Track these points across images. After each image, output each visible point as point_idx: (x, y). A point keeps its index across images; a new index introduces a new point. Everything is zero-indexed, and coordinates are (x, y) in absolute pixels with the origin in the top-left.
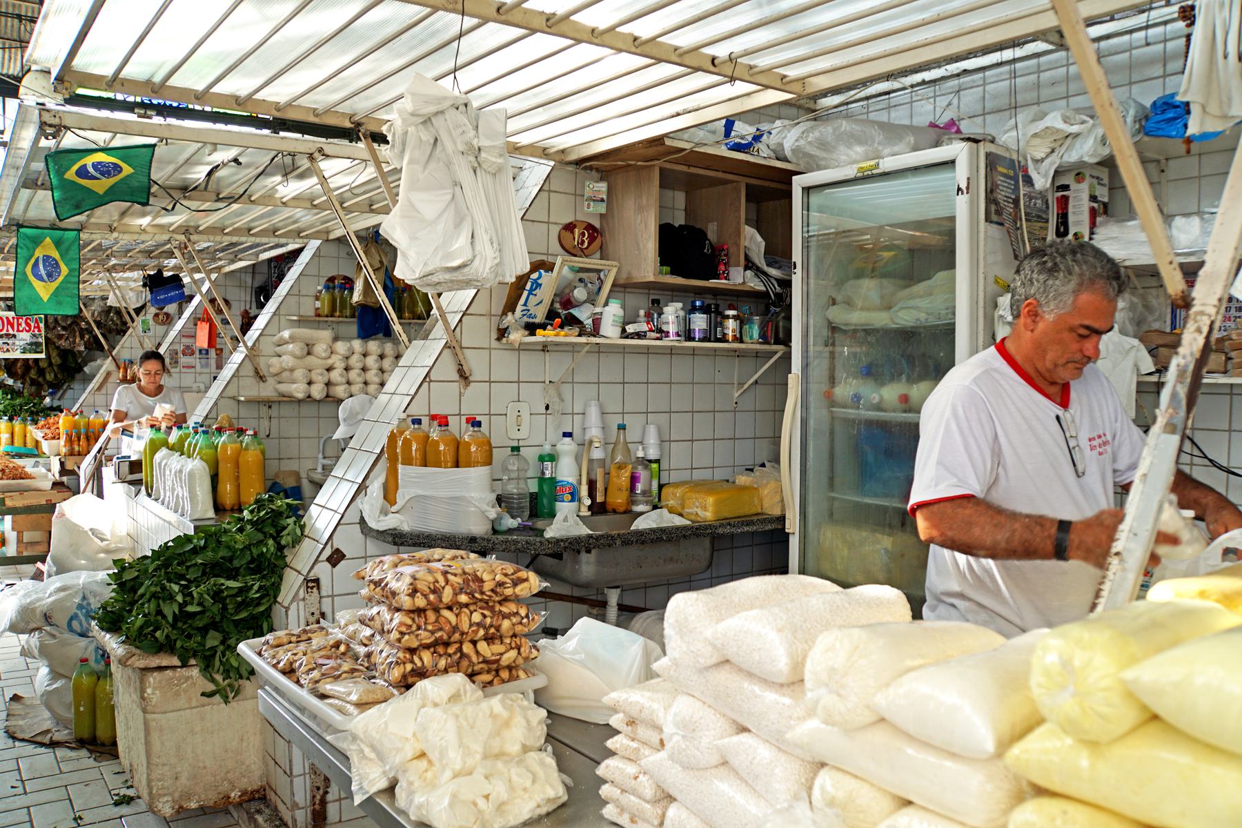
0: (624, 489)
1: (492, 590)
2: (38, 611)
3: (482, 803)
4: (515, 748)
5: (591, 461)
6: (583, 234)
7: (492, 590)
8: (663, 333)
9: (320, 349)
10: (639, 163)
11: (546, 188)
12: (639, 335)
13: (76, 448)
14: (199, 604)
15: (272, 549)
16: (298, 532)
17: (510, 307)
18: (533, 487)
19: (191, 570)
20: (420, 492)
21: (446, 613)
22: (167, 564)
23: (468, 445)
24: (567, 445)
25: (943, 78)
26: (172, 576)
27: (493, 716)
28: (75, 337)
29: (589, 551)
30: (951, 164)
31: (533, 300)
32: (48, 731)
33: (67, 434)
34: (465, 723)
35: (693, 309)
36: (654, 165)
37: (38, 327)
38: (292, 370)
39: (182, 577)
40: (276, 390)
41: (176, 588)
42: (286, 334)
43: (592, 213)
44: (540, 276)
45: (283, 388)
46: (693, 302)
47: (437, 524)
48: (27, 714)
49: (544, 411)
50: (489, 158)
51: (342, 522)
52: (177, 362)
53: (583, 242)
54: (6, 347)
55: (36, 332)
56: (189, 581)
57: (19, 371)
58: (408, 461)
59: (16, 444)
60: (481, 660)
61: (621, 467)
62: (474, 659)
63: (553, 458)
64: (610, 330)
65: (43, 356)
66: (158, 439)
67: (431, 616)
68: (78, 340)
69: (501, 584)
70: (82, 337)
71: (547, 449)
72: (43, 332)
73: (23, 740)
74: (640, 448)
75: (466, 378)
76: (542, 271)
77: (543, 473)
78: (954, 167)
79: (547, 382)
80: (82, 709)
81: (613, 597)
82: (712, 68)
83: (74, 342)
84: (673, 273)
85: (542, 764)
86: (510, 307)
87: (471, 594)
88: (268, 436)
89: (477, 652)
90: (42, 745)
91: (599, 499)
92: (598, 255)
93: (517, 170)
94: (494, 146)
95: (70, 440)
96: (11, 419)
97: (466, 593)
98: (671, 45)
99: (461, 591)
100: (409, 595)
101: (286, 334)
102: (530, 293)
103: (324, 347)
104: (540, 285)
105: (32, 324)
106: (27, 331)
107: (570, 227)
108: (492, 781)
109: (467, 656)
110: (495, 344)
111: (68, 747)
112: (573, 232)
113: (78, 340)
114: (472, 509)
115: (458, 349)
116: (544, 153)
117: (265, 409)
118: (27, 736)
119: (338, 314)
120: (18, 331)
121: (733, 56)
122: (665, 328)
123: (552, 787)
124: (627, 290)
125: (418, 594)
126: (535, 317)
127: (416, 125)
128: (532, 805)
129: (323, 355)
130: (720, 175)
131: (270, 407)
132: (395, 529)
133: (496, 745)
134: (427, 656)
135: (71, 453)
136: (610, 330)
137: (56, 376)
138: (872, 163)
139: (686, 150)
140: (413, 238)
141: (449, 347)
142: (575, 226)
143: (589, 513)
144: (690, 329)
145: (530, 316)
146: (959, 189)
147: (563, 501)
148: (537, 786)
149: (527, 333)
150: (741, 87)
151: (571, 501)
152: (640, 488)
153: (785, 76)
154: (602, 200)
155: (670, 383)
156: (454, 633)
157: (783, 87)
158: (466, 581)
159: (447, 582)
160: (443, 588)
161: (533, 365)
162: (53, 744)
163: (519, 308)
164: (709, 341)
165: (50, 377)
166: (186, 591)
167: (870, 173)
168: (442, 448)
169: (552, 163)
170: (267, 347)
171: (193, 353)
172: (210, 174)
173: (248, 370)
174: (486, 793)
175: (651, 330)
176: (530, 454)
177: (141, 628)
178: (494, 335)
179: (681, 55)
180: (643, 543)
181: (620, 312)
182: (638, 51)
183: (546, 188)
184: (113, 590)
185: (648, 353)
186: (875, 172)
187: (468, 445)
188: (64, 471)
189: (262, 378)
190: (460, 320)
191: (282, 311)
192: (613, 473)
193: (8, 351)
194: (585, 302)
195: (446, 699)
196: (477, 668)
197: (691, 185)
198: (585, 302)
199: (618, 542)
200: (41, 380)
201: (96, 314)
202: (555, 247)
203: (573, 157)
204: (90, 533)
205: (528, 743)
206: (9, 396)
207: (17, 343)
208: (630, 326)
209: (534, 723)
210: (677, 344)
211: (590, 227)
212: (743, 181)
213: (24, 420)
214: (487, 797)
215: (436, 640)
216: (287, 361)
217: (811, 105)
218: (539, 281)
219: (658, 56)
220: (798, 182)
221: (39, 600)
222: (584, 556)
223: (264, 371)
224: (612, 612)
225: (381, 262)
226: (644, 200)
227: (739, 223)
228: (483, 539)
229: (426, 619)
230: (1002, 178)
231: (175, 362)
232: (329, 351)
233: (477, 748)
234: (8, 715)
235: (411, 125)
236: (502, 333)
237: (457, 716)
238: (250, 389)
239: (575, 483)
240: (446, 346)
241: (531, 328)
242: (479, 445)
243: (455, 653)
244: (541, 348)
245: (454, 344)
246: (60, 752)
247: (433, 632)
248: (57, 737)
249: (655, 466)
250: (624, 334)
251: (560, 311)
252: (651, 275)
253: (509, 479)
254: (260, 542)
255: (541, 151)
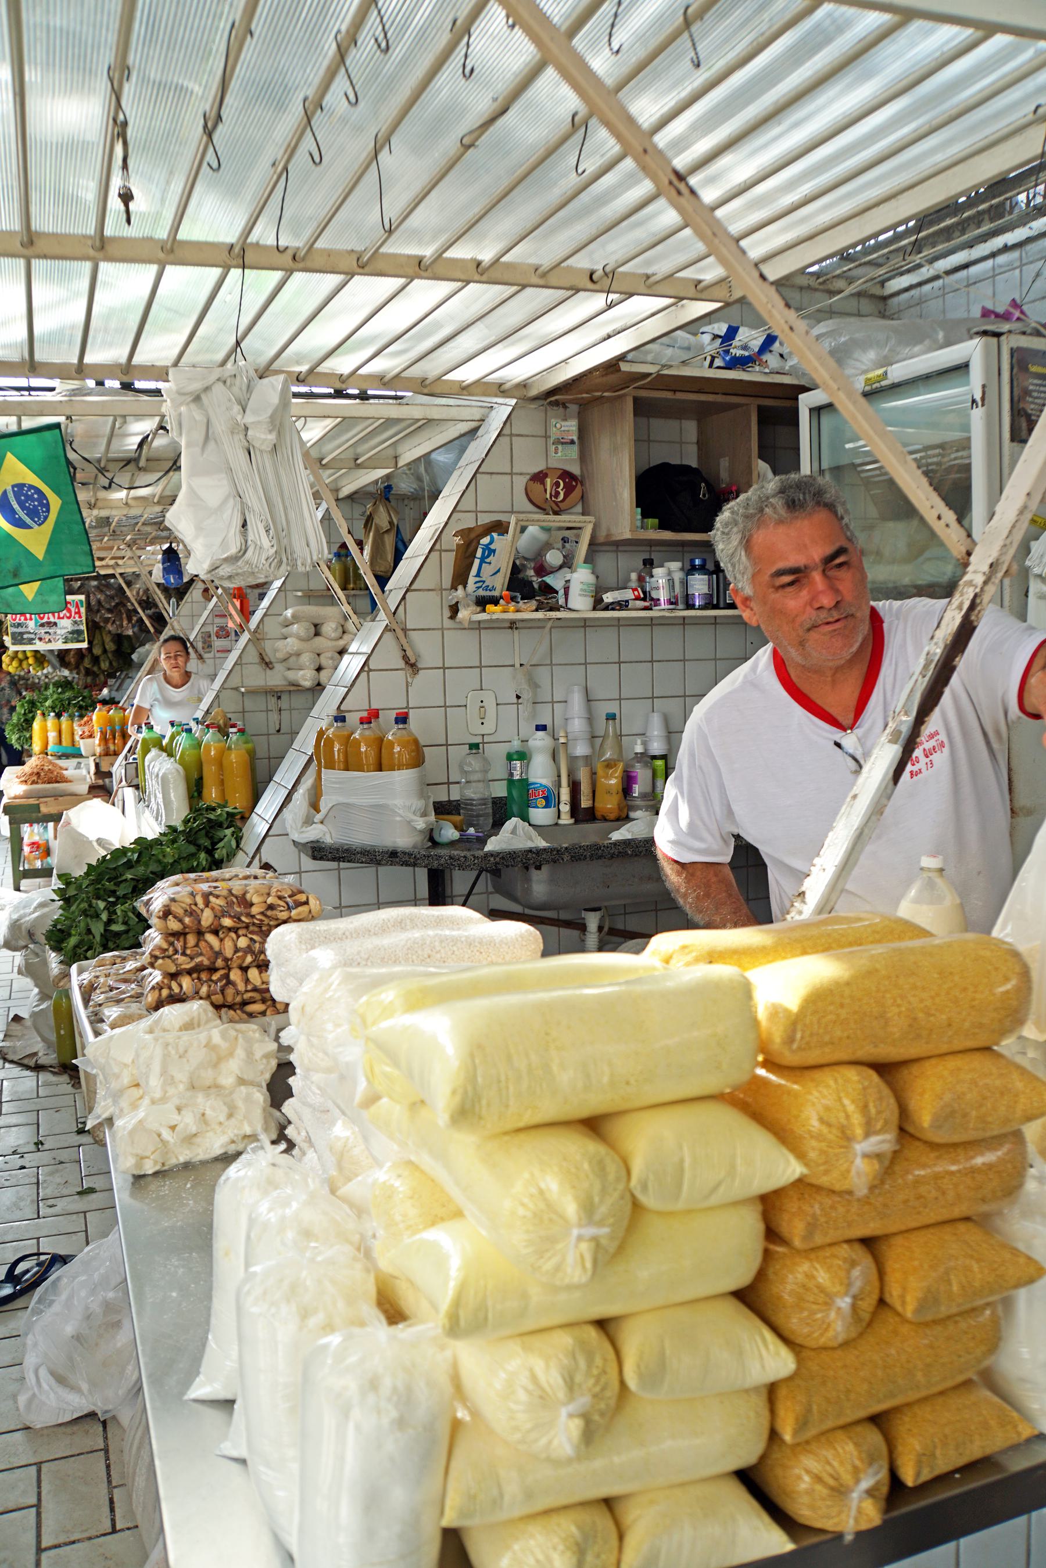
0: (614, 791)
1: (262, 913)
2: (23, 928)
3: (166, 1134)
4: (227, 1081)
5: (572, 760)
6: (557, 485)
7: (262, 913)
8: (647, 598)
9: (329, 628)
10: (606, 394)
11: (507, 431)
12: (623, 605)
13: (112, 747)
14: (125, 923)
15: (204, 863)
16: (234, 843)
17: (460, 578)
18: (500, 790)
19: (122, 885)
20: (342, 799)
21: (210, 938)
22: (98, 881)
23: (391, 744)
24: (540, 741)
25: (1029, 240)
26: (102, 892)
27: (209, 1046)
28: (121, 620)
29: (538, 868)
30: (963, 368)
31: (487, 570)
32: (35, 1054)
33: (101, 732)
34: (173, 1052)
35: (692, 570)
36: (624, 395)
37: (79, 613)
38: (298, 655)
39: (113, 893)
40: (285, 678)
41: (101, 905)
42: (289, 613)
43: (567, 459)
44: (492, 542)
45: (292, 675)
46: (692, 561)
47: (361, 837)
48: (23, 1035)
49: (515, 700)
50: (258, 435)
51: (270, 833)
52: (210, 646)
53: (557, 494)
54: (47, 637)
55: (77, 618)
56: (118, 898)
57: (72, 660)
58: (330, 766)
59: (64, 743)
60: (249, 987)
61: (609, 765)
62: (241, 987)
63: (523, 756)
64: (580, 602)
65: (84, 645)
66: (151, 739)
67: (191, 940)
68: (125, 623)
69: (271, 907)
70: (130, 620)
71: (516, 745)
72: (84, 618)
73: (12, 1062)
74: (639, 742)
75: (413, 665)
76: (495, 535)
77: (511, 775)
78: (968, 373)
79: (517, 665)
80: (62, 1032)
81: (592, 921)
82: (590, 286)
83: (122, 626)
84: (662, 526)
85: (248, 1099)
86: (460, 578)
87: (237, 918)
88: (279, 731)
89: (247, 981)
90: (27, 1067)
91: (585, 803)
92: (579, 508)
93: (487, 410)
94: (259, 422)
95: (104, 739)
96: (58, 716)
97: (230, 917)
98: (529, 265)
99: (224, 914)
100: (159, 918)
101: (289, 613)
102: (482, 561)
103: (333, 625)
104: (494, 551)
105: (73, 610)
106: (69, 618)
107: (539, 477)
108: (183, 1112)
109: (234, 984)
110: (448, 623)
111: (51, 1072)
112: (543, 483)
113: (125, 623)
114: (398, 819)
115: (398, 631)
116: (501, 389)
117: (274, 700)
118: (16, 1058)
119: (352, 586)
120: (59, 618)
121: (608, 269)
122: (654, 595)
123: (250, 1124)
124: (620, 548)
125: (170, 917)
126: (493, 589)
127: (188, 404)
128: (224, 1139)
129: (333, 635)
130: (720, 398)
131: (279, 698)
132: (318, 841)
133: (207, 1076)
134: (186, 982)
135: (107, 753)
136: (580, 602)
137: (111, 663)
138: (880, 371)
139: (651, 374)
140: (199, 529)
141: (390, 630)
142: (546, 475)
143: (572, 821)
144: (687, 595)
145: (487, 588)
146: (974, 401)
147: (536, 807)
148: (233, 1121)
149: (479, 609)
150: (641, 305)
151: (545, 807)
152: (637, 790)
153: (700, 282)
154: (572, 442)
155: (684, 660)
156: (216, 958)
157: (699, 296)
158: (230, 904)
159: (207, 904)
160: (202, 911)
161: (497, 646)
162: (38, 1068)
163: (471, 580)
164: (716, 607)
165: (104, 665)
166: (111, 909)
167: (877, 385)
168: (363, 749)
169: (513, 402)
170: (272, 628)
171: (227, 635)
172: (141, 445)
173: (252, 656)
174: (173, 1124)
175: (637, 598)
176: (496, 753)
177: (76, 947)
178: (447, 613)
179: (544, 275)
180: (600, 857)
181: (590, 579)
182: (484, 278)
183: (507, 431)
184: (61, 907)
185: (652, 625)
186: (884, 383)
187: (391, 744)
188: (99, 773)
189: (268, 665)
190: (404, 598)
191: (288, 586)
192: (600, 772)
193: (50, 641)
194: (561, 567)
195: (177, 1026)
196: (247, 996)
197: (702, 413)
198: (561, 567)
199: (566, 857)
200: (95, 669)
201: (141, 593)
202: (521, 502)
203: (534, 392)
204: (95, 844)
205: (245, 1077)
206: (60, 690)
207: (59, 632)
208: (608, 594)
209: (258, 1053)
210: (667, 614)
211: (566, 475)
212: (753, 404)
213: (71, 717)
214: (173, 1128)
215: (197, 965)
216: (292, 644)
217: (877, 291)
218: (492, 547)
219: (522, 282)
220: (806, 402)
221: (25, 915)
222: (535, 874)
223: (270, 656)
224: (592, 937)
225: (391, 523)
226: (619, 438)
227: (750, 457)
228: (404, 853)
229: (185, 943)
230: (1036, 381)
231: (208, 646)
232: (340, 630)
233: (181, 1076)
234: (5, 1036)
235: (181, 404)
236: (454, 609)
237: (167, 1045)
238: (257, 679)
239: (550, 785)
240: (387, 629)
241: (482, 603)
242: (403, 745)
243: (220, 980)
244: (508, 625)
245: (394, 626)
246: (44, 1076)
247: (192, 958)
248: (43, 1060)
249: (660, 763)
250: (598, 604)
251: (535, 579)
252: (628, 530)
253: (467, 782)
254: (193, 855)
255: (495, 389)
